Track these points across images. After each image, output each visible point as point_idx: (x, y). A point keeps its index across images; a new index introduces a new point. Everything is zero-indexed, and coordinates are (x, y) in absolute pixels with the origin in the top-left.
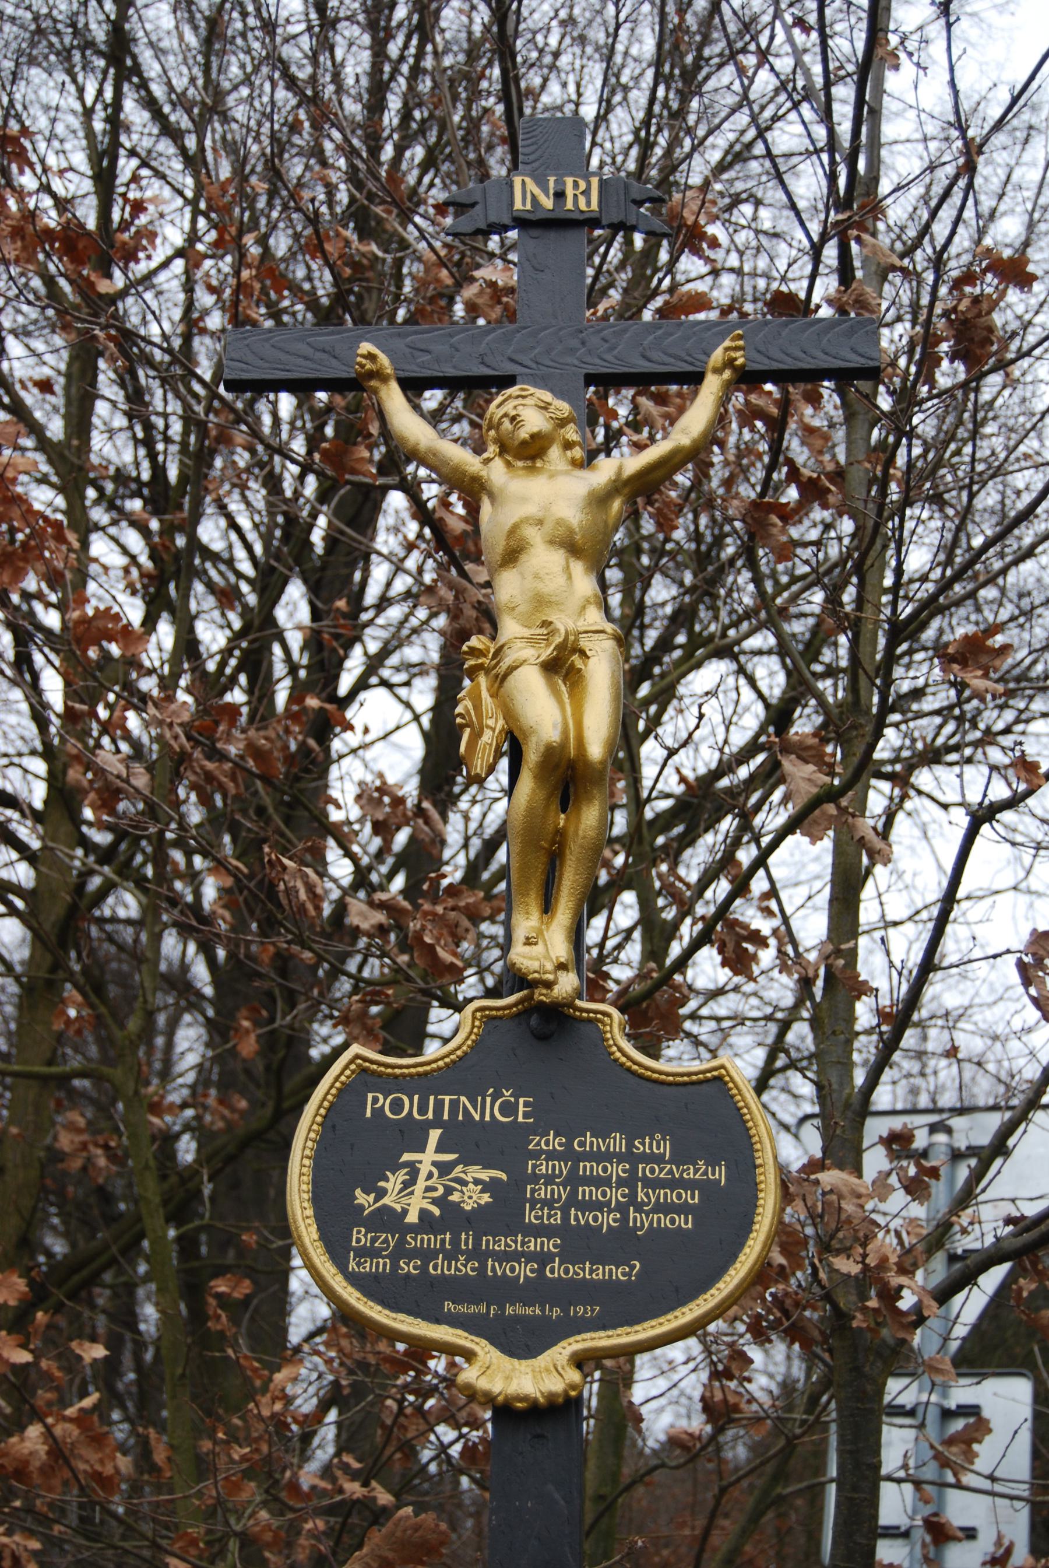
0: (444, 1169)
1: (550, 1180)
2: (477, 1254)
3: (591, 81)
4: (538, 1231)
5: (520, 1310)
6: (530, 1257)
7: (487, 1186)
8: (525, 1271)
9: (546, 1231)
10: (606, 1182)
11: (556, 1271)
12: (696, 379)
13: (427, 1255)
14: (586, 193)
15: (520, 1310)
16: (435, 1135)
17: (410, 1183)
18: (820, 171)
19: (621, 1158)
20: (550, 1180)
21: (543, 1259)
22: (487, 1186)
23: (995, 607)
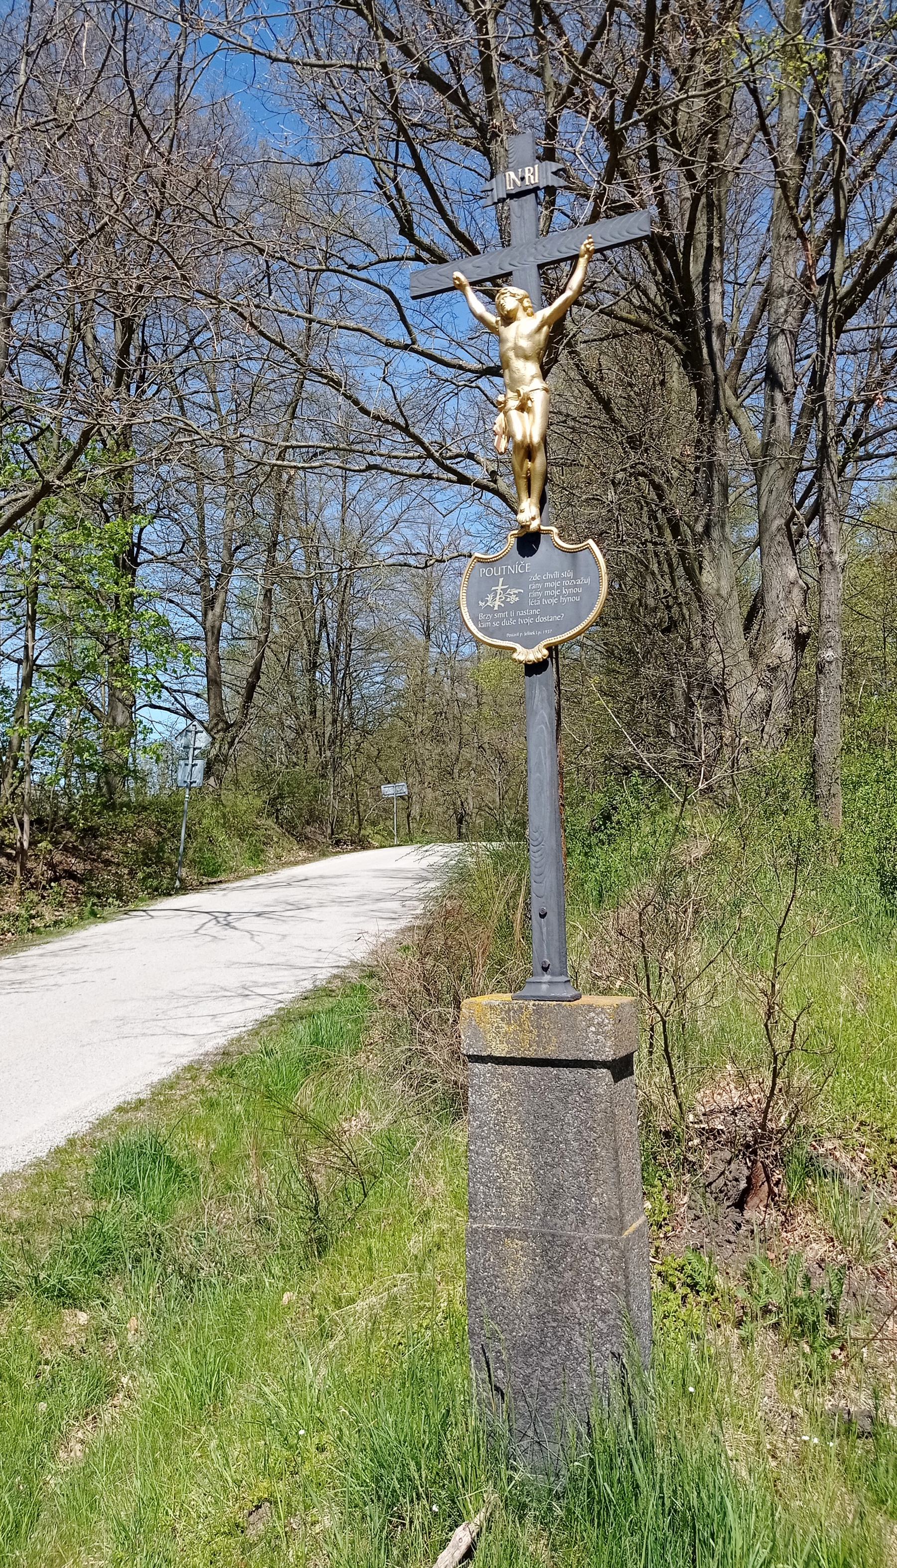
0: (504, 590)
1: (536, 590)
2: (516, 617)
3: (696, 258)
4: (533, 607)
5: (529, 633)
6: (531, 616)
7: (517, 595)
8: (530, 621)
9: (536, 607)
10: (553, 588)
11: (539, 620)
12: (575, 259)
13: (501, 619)
14: (533, 174)
15: (529, 633)
16: (501, 580)
17: (495, 597)
18: (878, 464)
19: (557, 580)
20: (536, 590)
21: (535, 616)
22: (517, 595)
23: (20, 655)
